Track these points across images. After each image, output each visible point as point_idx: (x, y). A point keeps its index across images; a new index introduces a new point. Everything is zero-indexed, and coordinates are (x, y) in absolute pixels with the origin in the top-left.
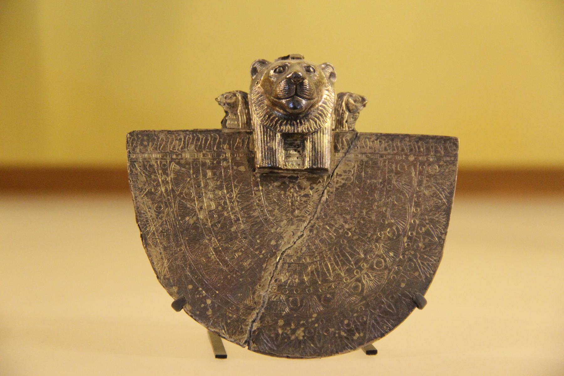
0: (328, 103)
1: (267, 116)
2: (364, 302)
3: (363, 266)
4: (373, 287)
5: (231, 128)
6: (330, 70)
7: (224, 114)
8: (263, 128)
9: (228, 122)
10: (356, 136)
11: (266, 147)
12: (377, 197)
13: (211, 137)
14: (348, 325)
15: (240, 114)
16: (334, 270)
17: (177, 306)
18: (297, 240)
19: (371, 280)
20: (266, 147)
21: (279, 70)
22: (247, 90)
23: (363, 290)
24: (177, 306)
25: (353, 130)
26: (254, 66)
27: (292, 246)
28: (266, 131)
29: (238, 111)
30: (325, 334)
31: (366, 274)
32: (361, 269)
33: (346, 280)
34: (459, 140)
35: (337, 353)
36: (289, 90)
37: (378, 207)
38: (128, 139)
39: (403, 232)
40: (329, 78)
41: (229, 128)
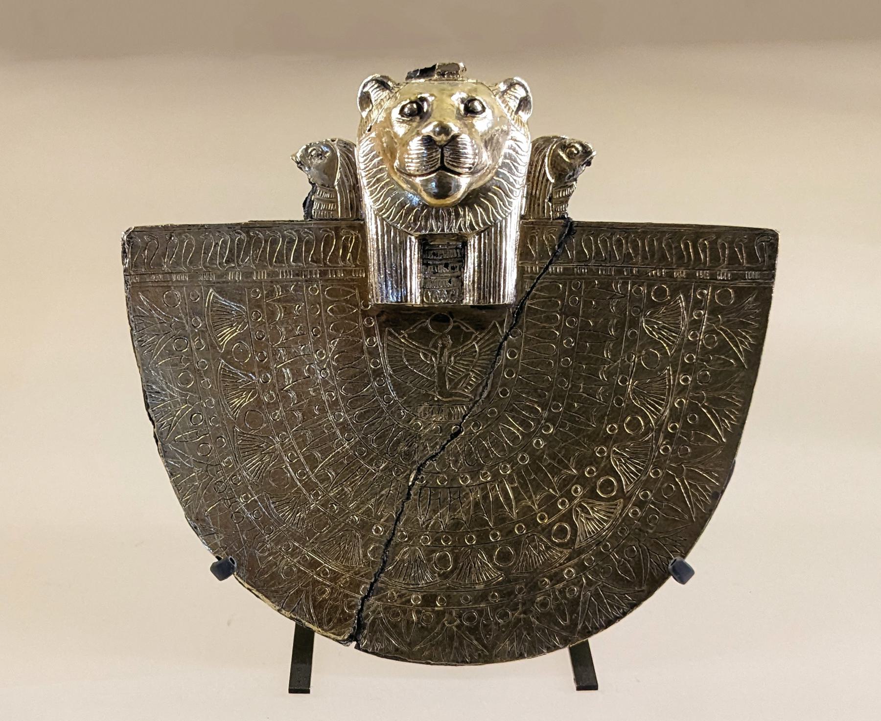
0: (518, 160)
1: (389, 199)
2: (576, 560)
3: (576, 491)
4: (594, 532)
5: (321, 220)
6: (520, 93)
7: (311, 187)
8: (382, 224)
9: (316, 206)
10: (571, 228)
11: (398, 239)
12: (317, 455)
13: (284, 237)
14: (544, 604)
15: (339, 188)
16: (518, 499)
17: (222, 570)
18: (448, 441)
19: (589, 519)
20: (398, 239)
21: (410, 109)
22: (352, 138)
23: (573, 541)
24: (222, 570)
25: (563, 218)
26: (365, 90)
27: (437, 454)
28: (387, 231)
29: (336, 183)
30: (500, 621)
31: (581, 506)
32: (571, 499)
33: (542, 519)
34: (779, 234)
35: (521, 656)
36: (430, 158)
37: (609, 374)
38: (124, 244)
39: (656, 423)
40: (517, 112)
41: (316, 220)
